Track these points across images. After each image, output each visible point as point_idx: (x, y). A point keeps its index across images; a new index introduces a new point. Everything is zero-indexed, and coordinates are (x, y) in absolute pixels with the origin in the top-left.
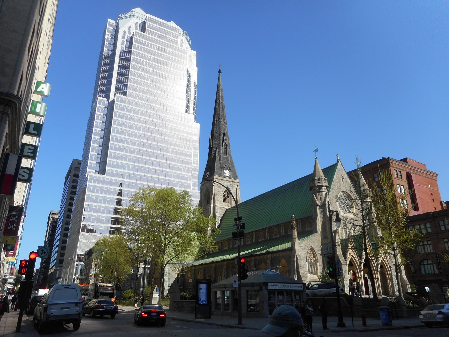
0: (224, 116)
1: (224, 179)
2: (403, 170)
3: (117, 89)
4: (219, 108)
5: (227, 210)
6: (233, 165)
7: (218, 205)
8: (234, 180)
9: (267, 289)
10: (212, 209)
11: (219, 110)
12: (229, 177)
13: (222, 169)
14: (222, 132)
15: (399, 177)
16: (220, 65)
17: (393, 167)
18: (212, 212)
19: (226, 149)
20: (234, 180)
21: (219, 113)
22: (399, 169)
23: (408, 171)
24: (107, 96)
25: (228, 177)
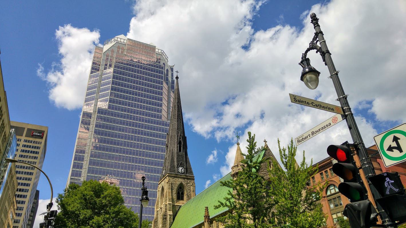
16: (177, 72)
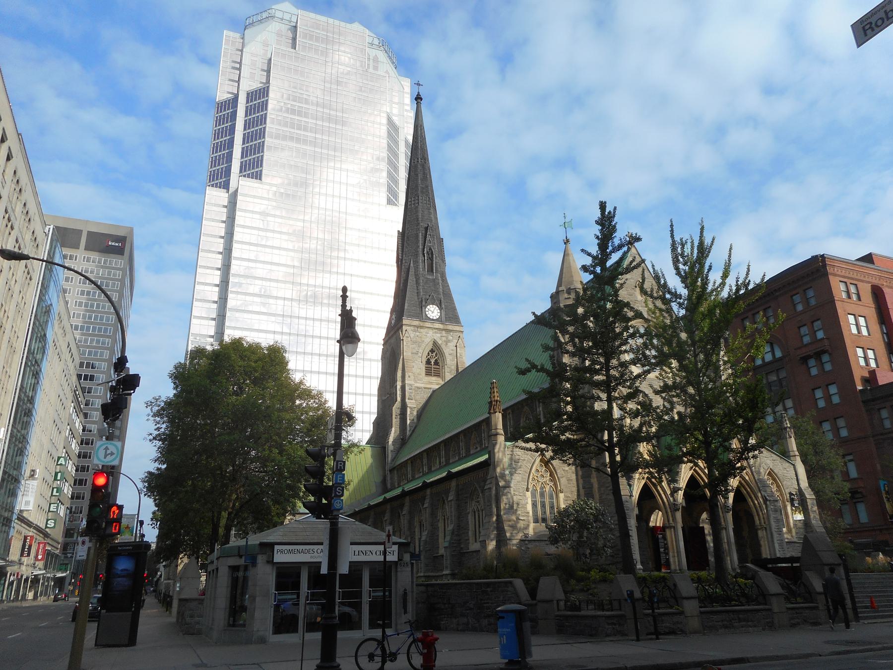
0: (427, 191)
1: (428, 325)
2: (862, 281)
3: (243, 168)
4: (417, 175)
5: (434, 391)
6: (448, 295)
7: (412, 382)
8: (450, 327)
9: (270, 561)
10: (399, 393)
11: (417, 180)
12: (439, 320)
13: (422, 305)
14: (423, 225)
15: (854, 297)
16: (419, 84)
17: (835, 275)
18: (399, 399)
19: (432, 260)
20: (450, 327)
21: (417, 186)
22: (852, 279)
23: (876, 282)
24: (226, 186)
25: (437, 320)
